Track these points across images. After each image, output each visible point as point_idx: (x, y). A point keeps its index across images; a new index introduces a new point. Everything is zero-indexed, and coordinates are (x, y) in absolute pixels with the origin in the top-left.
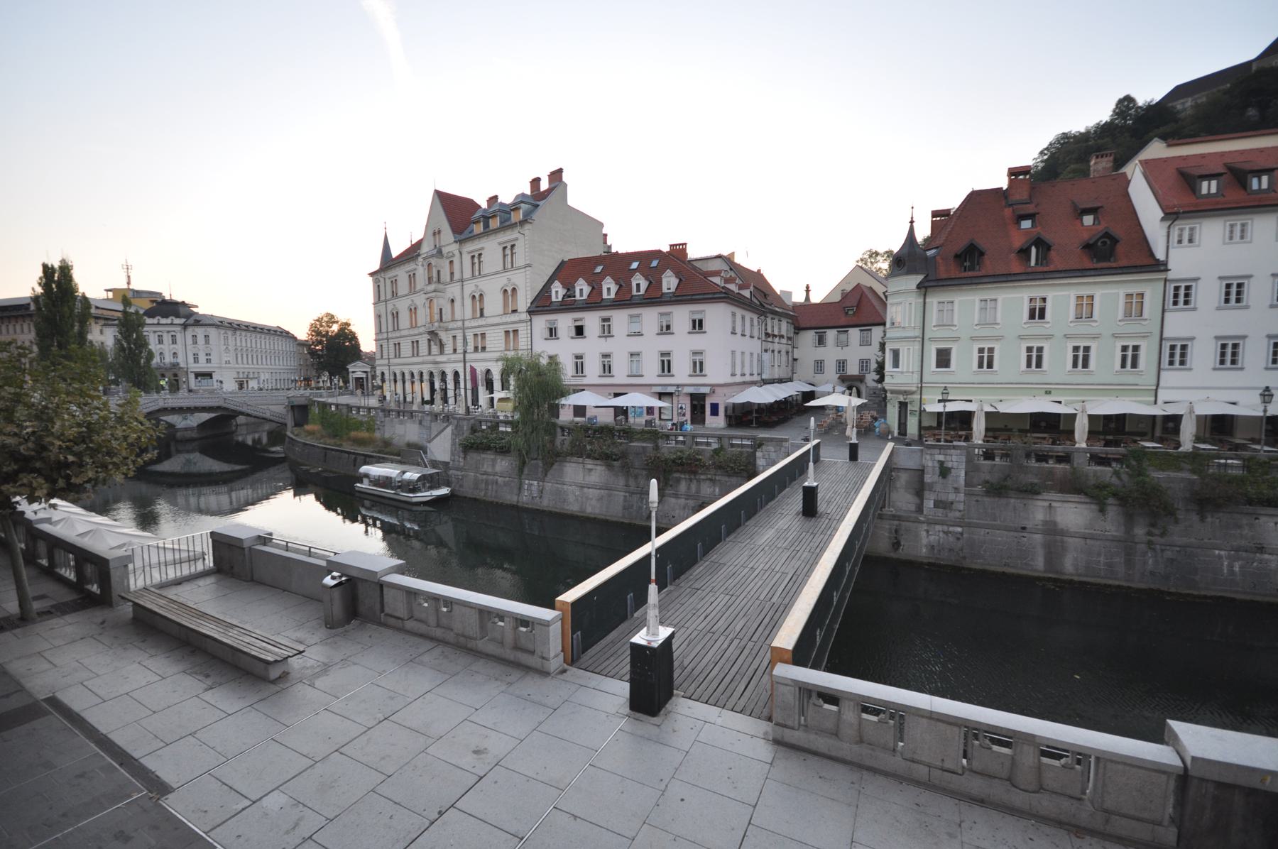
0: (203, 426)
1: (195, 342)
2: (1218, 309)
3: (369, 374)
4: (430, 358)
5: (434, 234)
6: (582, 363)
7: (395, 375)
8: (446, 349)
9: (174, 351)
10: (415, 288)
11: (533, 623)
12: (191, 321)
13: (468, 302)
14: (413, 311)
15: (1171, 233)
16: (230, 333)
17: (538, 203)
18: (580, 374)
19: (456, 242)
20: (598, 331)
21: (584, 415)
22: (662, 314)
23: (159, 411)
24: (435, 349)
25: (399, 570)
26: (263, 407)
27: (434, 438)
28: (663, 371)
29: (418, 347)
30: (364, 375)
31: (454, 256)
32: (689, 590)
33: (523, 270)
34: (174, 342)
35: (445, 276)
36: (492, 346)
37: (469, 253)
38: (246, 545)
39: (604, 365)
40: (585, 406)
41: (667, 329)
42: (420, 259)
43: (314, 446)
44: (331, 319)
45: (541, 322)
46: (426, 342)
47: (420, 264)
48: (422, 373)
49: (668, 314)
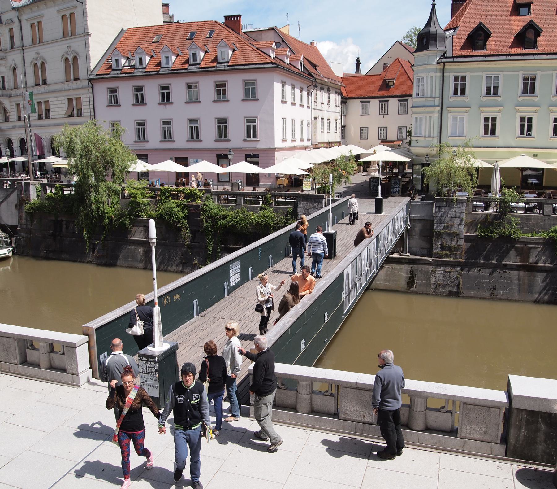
2: (159, 104)
13: (30, 71)
15: (25, 83)
25: (390, 421)
36: (56, 113)
39: (165, 132)
40: (188, 172)
41: (193, 100)
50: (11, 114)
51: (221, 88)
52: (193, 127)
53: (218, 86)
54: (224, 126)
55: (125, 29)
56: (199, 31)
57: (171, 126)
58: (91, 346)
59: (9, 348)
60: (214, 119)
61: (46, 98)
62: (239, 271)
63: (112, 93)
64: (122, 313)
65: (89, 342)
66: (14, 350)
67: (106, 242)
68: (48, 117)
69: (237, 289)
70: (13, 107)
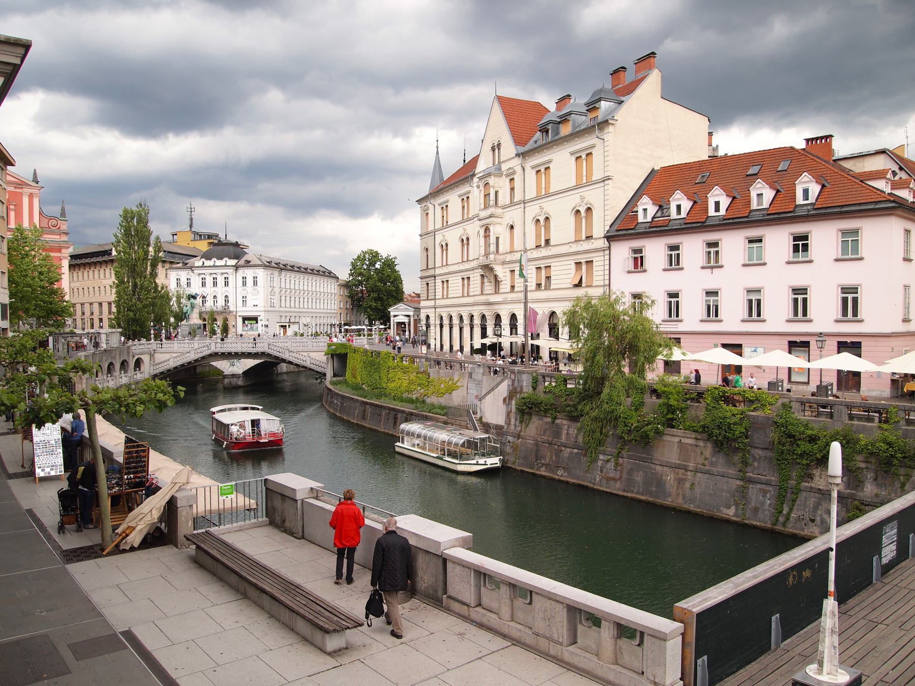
0: (247, 373)
1: (244, 284)
3: (412, 319)
4: (483, 298)
5: (493, 149)
6: (678, 302)
7: (441, 318)
8: (501, 287)
9: (226, 294)
10: (468, 213)
11: (642, 634)
12: (242, 262)
13: (531, 228)
14: (465, 242)
16: (276, 273)
17: (623, 99)
18: (674, 317)
19: (518, 155)
20: (663, 262)
21: (678, 372)
22: (845, 233)
23: (210, 355)
24: (489, 287)
26: (303, 353)
27: (486, 395)
28: (796, 314)
29: (469, 285)
30: (406, 320)
31: (514, 173)
32: (863, 622)
33: (602, 184)
34: (226, 284)
35: (504, 198)
37: (533, 168)
38: (299, 496)
41: (755, 262)
42: (476, 180)
43: (353, 399)
44: (375, 256)
45: (622, 252)
46: (479, 278)
47: (475, 185)
48: (451, 317)
49: (855, 232)
50: (502, 283)
51: (801, 243)
52: (752, 300)
53: (796, 239)
54: (803, 298)
55: (656, 169)
56: (766, 163)
57: (718, 298)
58: (686, 643)
59: (554, 617)
60: (787, 288)
61: (547, 263)
62: (895, 539)
63: (671, 250)
64: (733, 592)
65: (683, 634)
66: (560, 622)
67: (621, 460)
68: (548, 287)
69: (892, 571)
70: (505, 274)
